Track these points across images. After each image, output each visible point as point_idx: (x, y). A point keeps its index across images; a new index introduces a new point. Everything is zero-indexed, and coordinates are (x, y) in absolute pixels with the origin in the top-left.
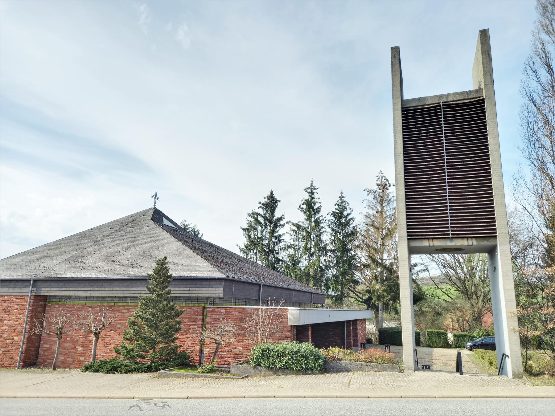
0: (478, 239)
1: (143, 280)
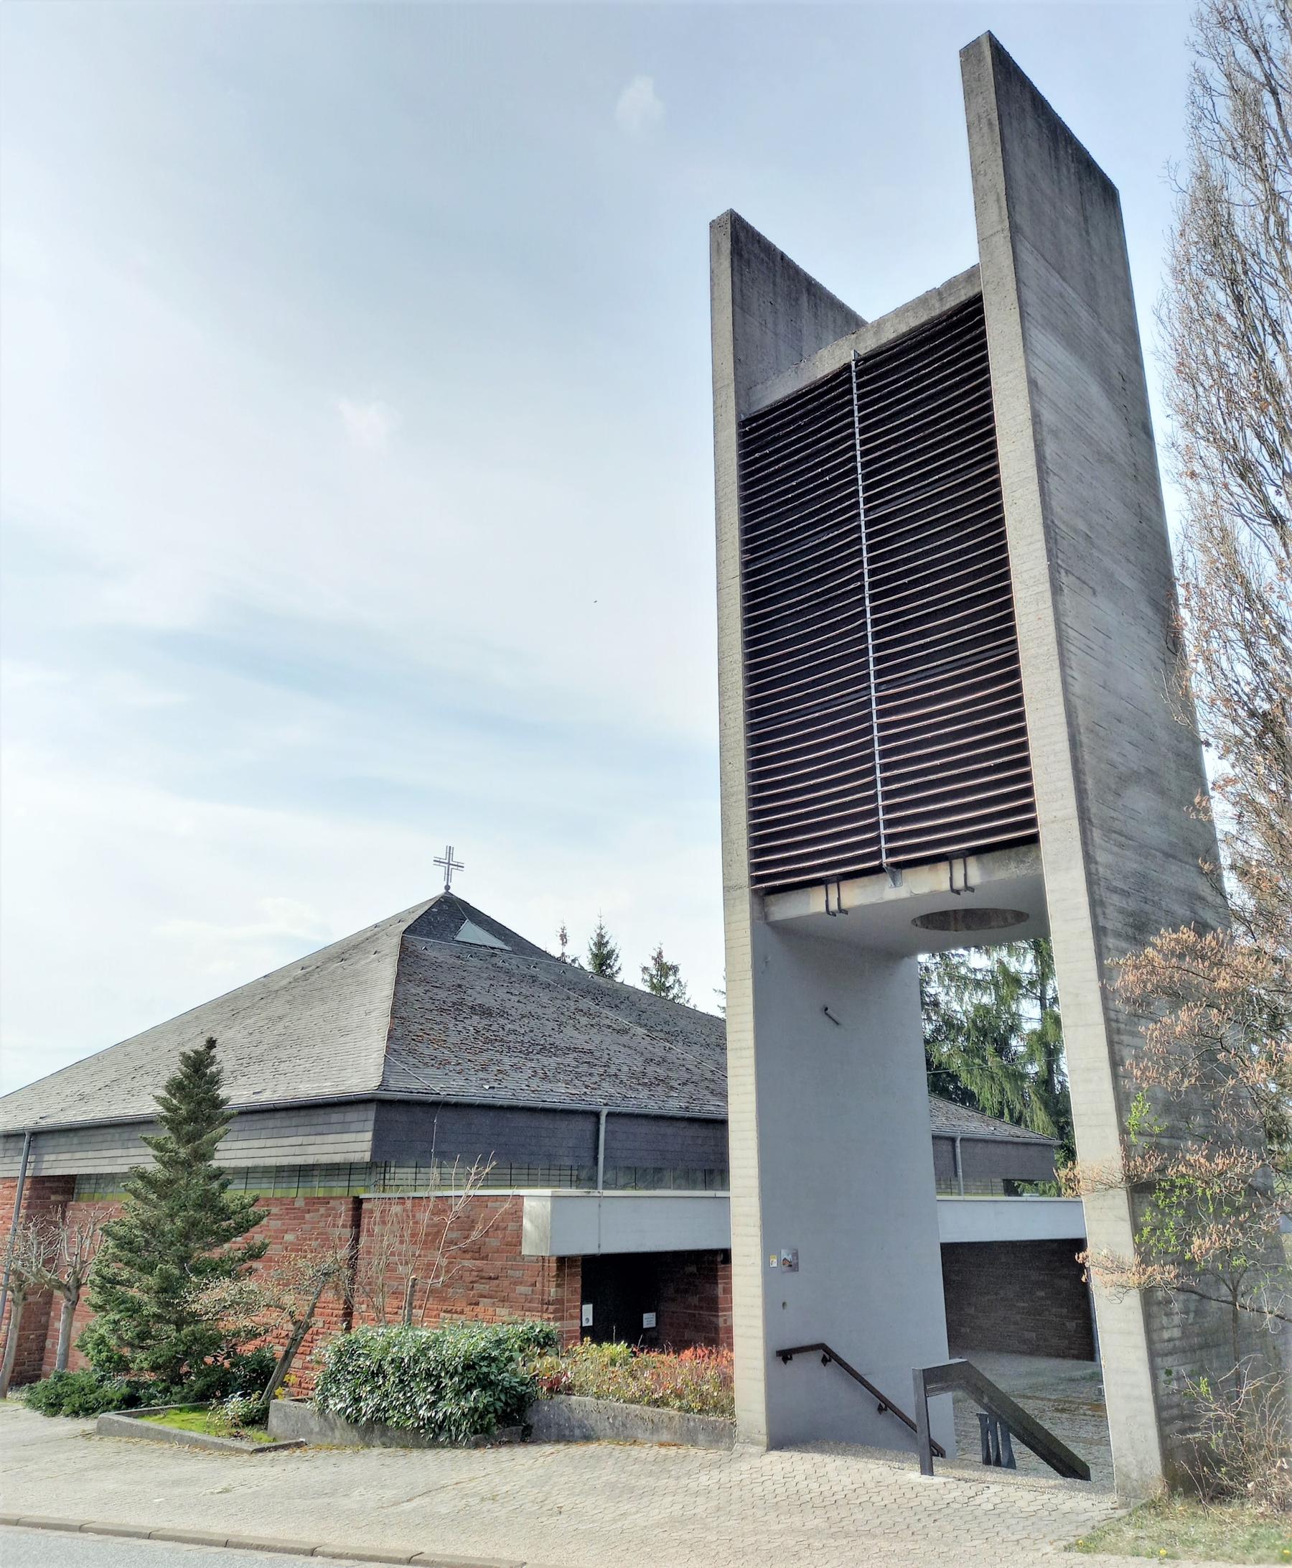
0: (987, 858)
1: (146, 1122)
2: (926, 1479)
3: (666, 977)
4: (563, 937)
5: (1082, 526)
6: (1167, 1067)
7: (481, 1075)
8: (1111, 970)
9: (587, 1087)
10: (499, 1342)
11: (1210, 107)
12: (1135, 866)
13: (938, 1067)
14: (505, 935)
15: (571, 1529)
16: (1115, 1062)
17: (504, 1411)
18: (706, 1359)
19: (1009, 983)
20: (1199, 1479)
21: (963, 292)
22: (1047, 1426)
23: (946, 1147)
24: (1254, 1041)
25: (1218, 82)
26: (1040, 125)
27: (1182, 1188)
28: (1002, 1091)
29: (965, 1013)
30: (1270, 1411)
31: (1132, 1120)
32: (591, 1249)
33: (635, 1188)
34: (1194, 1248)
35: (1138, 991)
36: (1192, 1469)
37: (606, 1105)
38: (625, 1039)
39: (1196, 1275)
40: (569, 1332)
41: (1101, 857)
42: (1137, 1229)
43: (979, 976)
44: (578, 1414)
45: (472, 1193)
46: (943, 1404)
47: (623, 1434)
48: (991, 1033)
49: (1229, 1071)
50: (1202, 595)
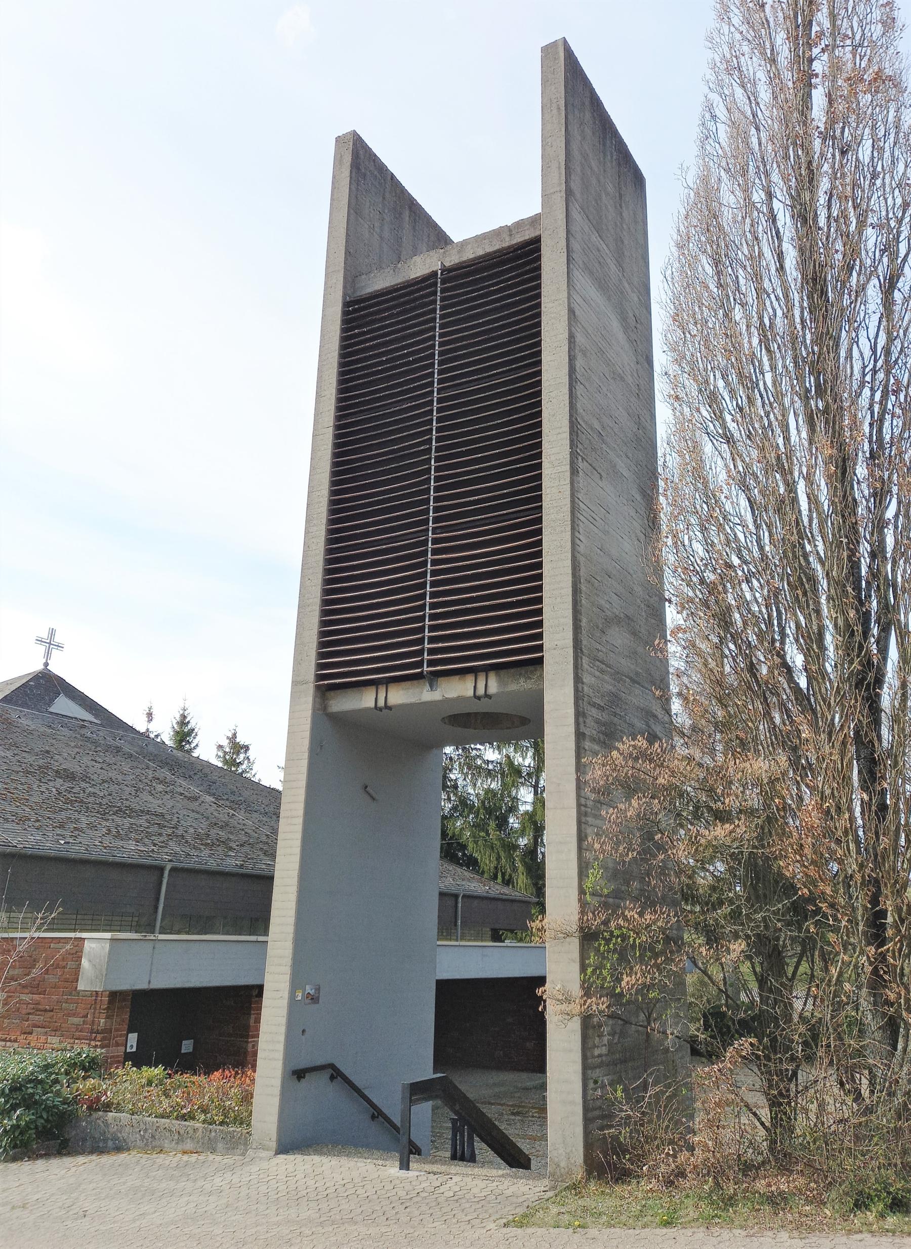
0: (502, 672)
2: (403, 1173)
3: (238, 755)
4: (150, 716)
5: (597, 425)
6: (618, 843)
7: (59, 831)
8: (585, 766)
9: (155, 845)
10: (47, 1066)
11: (714, 131)
12: (611, 687)
13: (451, 838)
14: (96, 710)
15: (93, 1230)
16: (581, 837)
17: (44, 1127)
18: (232, 1079)
19: (511, 773)
20: (608, 1163)
21: (527, 232)
22: (502, 1127)
23: (450, 902)
24: (682, 826)
25: (721, 112)
26: (594, 118)
27: (618, 937)
28: (498, 858)
29: (477, 795)
30: (664, 1111)
31: (588, 884)
32: (142, 985)
33: (188, 933)
34: (624, 984)
35: (602, 783)
36: (605, 1157)
37: (170, 861)
38: (194, 805)
39: (621, 1005)
40: (113, 1057)
41: (587, 679)
42: (583, 968)
43: (491, 767)
44: (113, 1129)
45: (36, 935)
46: (423, 1110)
47: (151, 1144)
48: (496, 811)
49: (661, 847)
50: (676, 489)
